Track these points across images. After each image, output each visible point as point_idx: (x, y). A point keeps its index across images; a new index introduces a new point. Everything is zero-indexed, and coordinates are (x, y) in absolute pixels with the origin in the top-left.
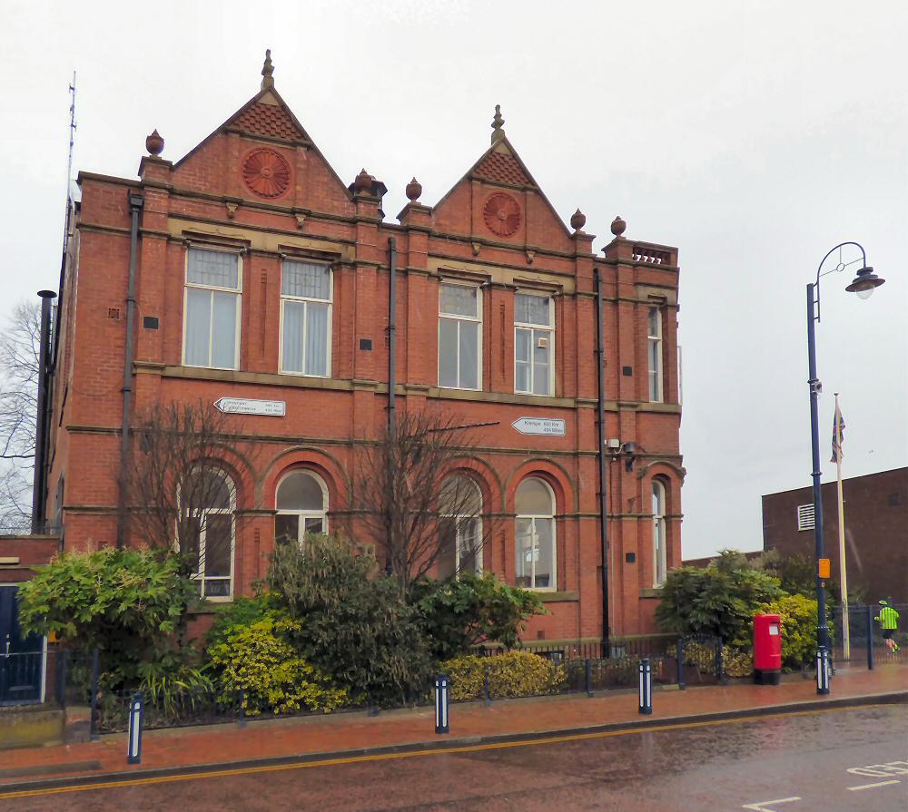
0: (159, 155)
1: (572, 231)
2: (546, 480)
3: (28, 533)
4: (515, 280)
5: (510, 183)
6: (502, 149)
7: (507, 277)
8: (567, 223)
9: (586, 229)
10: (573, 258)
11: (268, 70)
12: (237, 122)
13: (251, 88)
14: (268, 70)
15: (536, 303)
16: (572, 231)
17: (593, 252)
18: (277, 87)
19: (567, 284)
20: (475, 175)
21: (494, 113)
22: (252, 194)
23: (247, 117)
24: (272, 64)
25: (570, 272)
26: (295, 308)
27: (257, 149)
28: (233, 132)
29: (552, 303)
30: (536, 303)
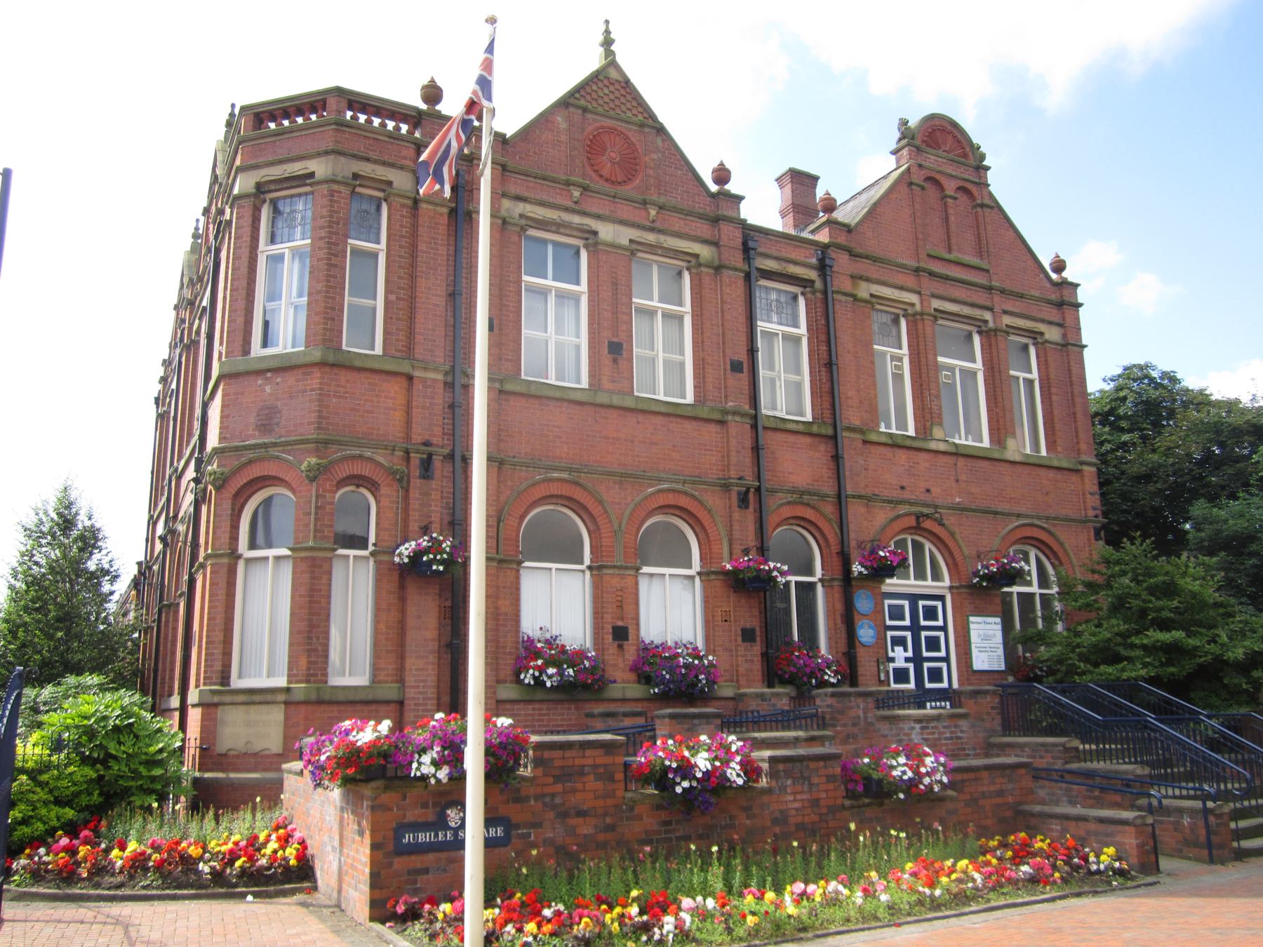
0: (438, 107)
1: (714, 188)
2: (817, 541)
3: (972, 619)
4: (631, 241)
5: (600, 109)
6: (613, 74)
7: (624, 235)
8: (1046, 264)
9: (732, 187)
10: (716, 220)
11: (608, 42)
12: (577, 96)
13: (592, 62)
14: (608, 42)
15: (783, 299)
16: (1054, 276)
17: (742, 216)
18: (619, 59)
19: (705, 252)
20: (572, 101)
21: (604, 28)
22: (598, 179)
23: (595, 88)
24: (612, 36)
25: (1057, 319)
26: (770, 335)
27: (597, 129)
28: (573, 106)
29: (687, 277)
30: (783, 299)
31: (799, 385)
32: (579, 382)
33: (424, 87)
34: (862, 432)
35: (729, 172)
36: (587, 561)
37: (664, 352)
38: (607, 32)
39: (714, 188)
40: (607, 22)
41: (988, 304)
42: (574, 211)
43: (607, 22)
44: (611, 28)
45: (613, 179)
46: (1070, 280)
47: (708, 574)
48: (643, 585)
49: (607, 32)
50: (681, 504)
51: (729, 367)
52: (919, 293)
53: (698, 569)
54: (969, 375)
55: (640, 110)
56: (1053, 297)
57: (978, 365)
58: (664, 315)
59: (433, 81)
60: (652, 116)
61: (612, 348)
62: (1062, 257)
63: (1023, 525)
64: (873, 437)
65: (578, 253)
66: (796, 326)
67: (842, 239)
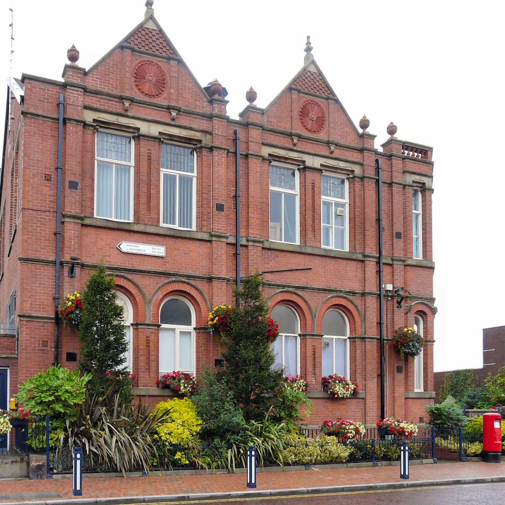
1: (361, 131)
9: (370, 130)
11: (308, 49)
13: (137, 18)
17: (227, 114)
18: (156, 16)
29: (347, 183)
30: (336, 183)
31: (343, 231)
32: (343, 248)
33: (69, 51)
34: (262, 242)
35: (255, 93)
36: (348, 335)
37: (323, 223)
38: (308, 43)
39: (361, 131)
40: (308, 37)
41: (209, 129)
42: (291, 150)
43: (308, 37)
44: (311, 41)
45: (150, 94)
46: (371, 133)
47: (199, 329)
48: (162, 335)
49: (308, 43)
50: (127, 287)
51: (394, 236)
52: (362, 165)
53: (132, 322)
54: (290, 198)
55: (168, 48)
56: (359, 146)
57: (297, 191)
58: (117, 170)
59: (251, 89)
60: (332, 93)
61: (311, 221)
62: (368, 118)
63: (174, 282)
64: (410, 262)
65: (293, 174)
66: (342, 197)
67: (76, 80)
